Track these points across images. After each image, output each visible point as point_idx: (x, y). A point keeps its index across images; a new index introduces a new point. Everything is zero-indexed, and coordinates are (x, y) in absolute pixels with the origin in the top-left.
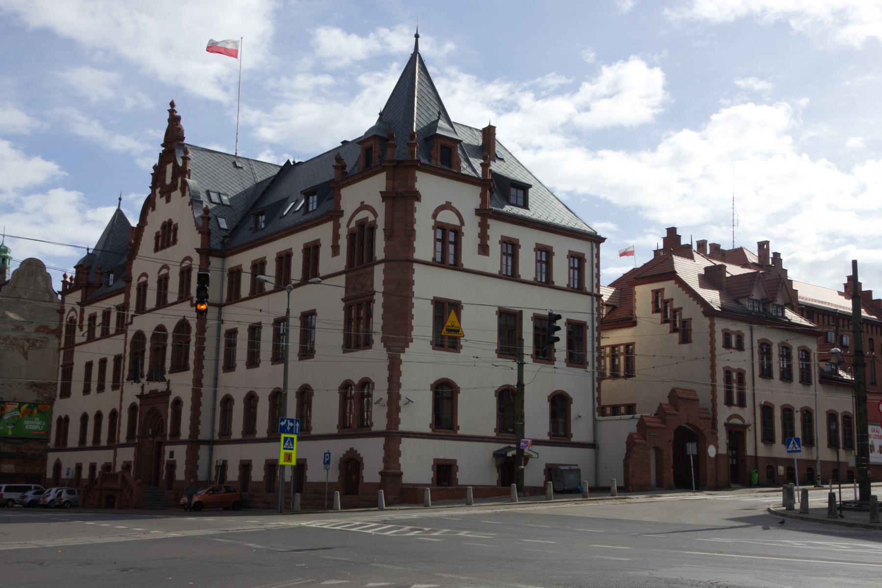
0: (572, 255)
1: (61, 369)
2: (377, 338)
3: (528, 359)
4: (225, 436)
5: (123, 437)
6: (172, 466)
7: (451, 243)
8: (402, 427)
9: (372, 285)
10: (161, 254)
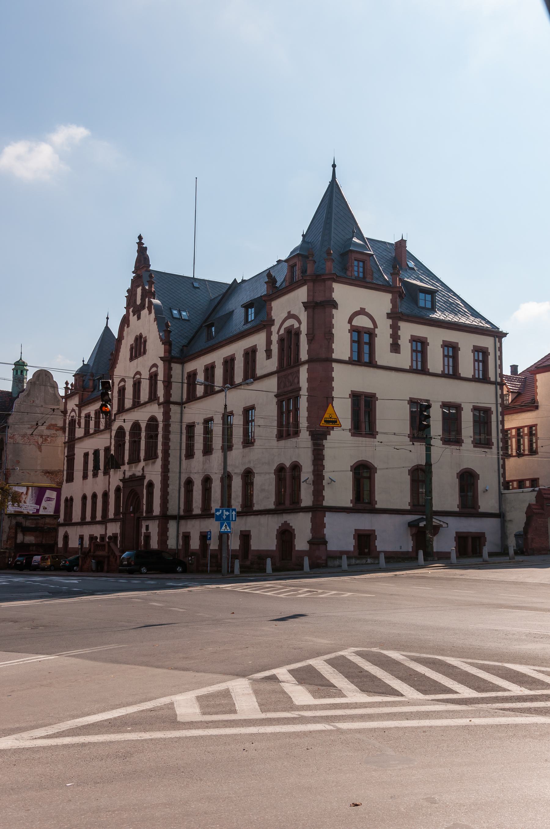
0: (477, 350)
1: (66, 459)
3: (436, 442)
4: (188, 515)
5: (111, 515)
6: (148, 537)
7: (366, 343)
9: (298, 382)
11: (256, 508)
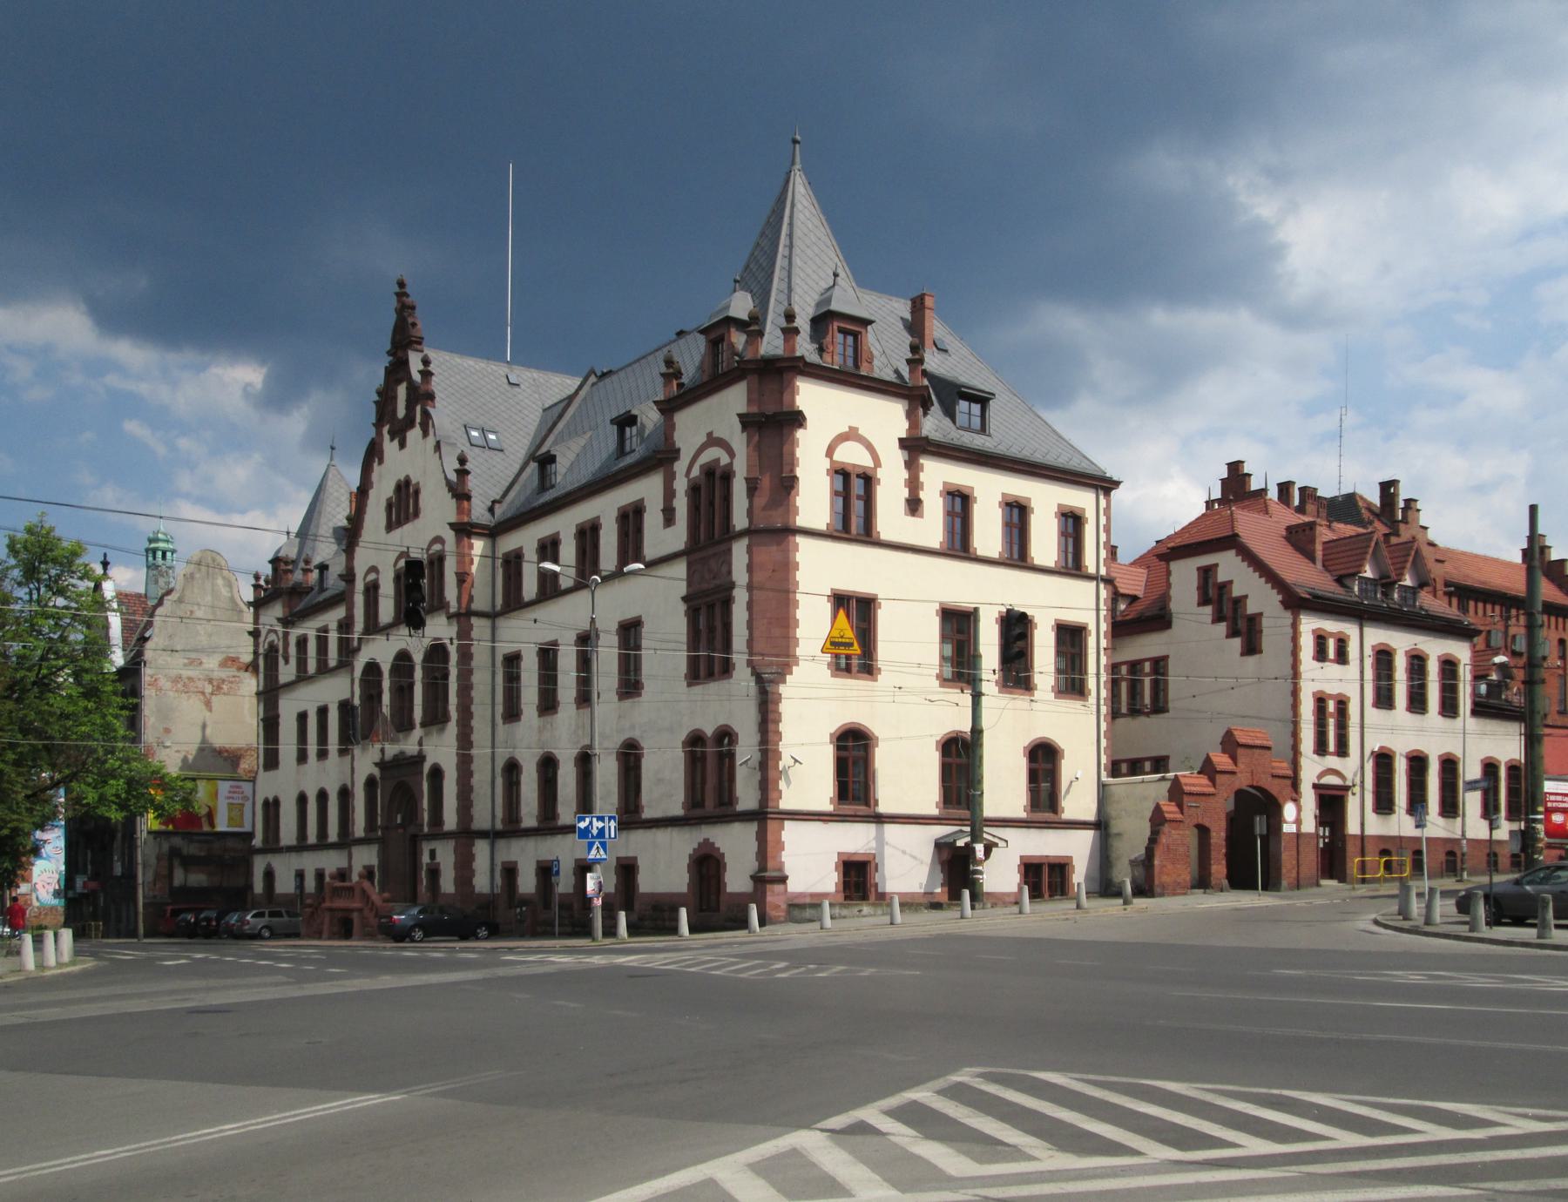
2: (739, 657)
4: (511, 829)
5: (359, 828)
6: (434, 873)
8: (785, 804)
9: (730, 572)
10: (397, 533)
11: (647, 814)
